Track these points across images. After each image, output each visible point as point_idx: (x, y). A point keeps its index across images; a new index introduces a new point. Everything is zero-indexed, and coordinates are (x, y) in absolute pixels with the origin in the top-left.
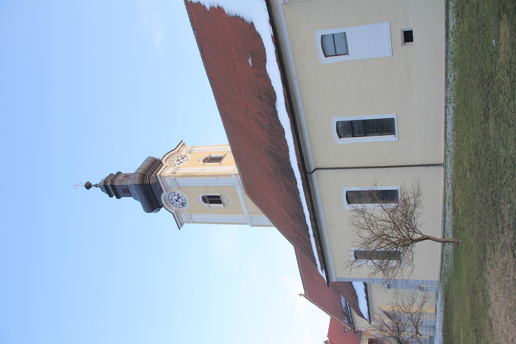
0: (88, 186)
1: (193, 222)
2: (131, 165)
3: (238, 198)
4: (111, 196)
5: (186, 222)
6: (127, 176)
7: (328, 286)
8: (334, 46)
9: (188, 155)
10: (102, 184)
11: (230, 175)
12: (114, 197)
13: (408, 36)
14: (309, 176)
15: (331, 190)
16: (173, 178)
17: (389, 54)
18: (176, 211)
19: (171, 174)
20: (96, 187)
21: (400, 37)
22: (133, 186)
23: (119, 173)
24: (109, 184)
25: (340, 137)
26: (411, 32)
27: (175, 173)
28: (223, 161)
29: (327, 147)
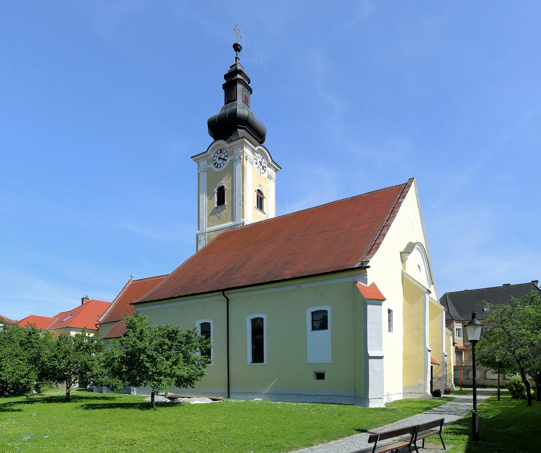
0: (237, 48)
1: (199, 174)
2: (252, 107)
3: (222, 223)
4: (226, 77)
5: (199, 166)
6: (246, 101)
7: (131, 304)
8: (320, 321)
9: (266, 174)
10: (239, 67)
11: (243, 217)
12: (224, 82)
13: (320, 376)
14: (221, 293)
15: (211, 311)
16: (241, 156)
17: (309, 361)
18: (209, 155)
19: (245, 154)
20: (236, 58)
21: (320, 370)
22: (234, 107)
23: (250, 90)
24: (239, 76)
25: (263, 319)
26: (323, 379)
27: (246, 160)
28: (259, 212)
29: (246, 309)
